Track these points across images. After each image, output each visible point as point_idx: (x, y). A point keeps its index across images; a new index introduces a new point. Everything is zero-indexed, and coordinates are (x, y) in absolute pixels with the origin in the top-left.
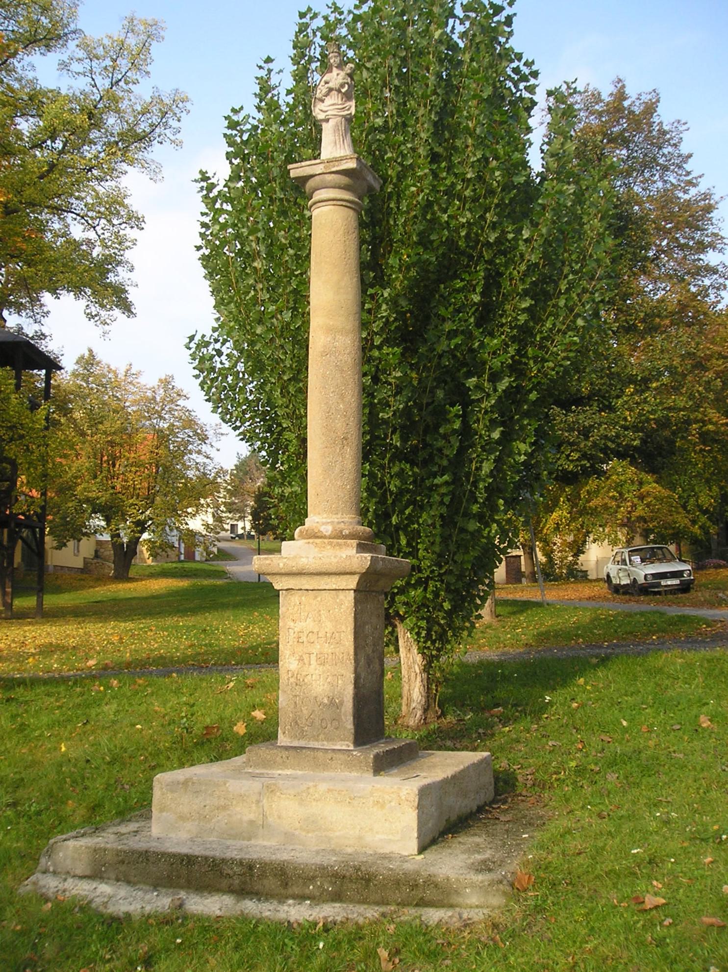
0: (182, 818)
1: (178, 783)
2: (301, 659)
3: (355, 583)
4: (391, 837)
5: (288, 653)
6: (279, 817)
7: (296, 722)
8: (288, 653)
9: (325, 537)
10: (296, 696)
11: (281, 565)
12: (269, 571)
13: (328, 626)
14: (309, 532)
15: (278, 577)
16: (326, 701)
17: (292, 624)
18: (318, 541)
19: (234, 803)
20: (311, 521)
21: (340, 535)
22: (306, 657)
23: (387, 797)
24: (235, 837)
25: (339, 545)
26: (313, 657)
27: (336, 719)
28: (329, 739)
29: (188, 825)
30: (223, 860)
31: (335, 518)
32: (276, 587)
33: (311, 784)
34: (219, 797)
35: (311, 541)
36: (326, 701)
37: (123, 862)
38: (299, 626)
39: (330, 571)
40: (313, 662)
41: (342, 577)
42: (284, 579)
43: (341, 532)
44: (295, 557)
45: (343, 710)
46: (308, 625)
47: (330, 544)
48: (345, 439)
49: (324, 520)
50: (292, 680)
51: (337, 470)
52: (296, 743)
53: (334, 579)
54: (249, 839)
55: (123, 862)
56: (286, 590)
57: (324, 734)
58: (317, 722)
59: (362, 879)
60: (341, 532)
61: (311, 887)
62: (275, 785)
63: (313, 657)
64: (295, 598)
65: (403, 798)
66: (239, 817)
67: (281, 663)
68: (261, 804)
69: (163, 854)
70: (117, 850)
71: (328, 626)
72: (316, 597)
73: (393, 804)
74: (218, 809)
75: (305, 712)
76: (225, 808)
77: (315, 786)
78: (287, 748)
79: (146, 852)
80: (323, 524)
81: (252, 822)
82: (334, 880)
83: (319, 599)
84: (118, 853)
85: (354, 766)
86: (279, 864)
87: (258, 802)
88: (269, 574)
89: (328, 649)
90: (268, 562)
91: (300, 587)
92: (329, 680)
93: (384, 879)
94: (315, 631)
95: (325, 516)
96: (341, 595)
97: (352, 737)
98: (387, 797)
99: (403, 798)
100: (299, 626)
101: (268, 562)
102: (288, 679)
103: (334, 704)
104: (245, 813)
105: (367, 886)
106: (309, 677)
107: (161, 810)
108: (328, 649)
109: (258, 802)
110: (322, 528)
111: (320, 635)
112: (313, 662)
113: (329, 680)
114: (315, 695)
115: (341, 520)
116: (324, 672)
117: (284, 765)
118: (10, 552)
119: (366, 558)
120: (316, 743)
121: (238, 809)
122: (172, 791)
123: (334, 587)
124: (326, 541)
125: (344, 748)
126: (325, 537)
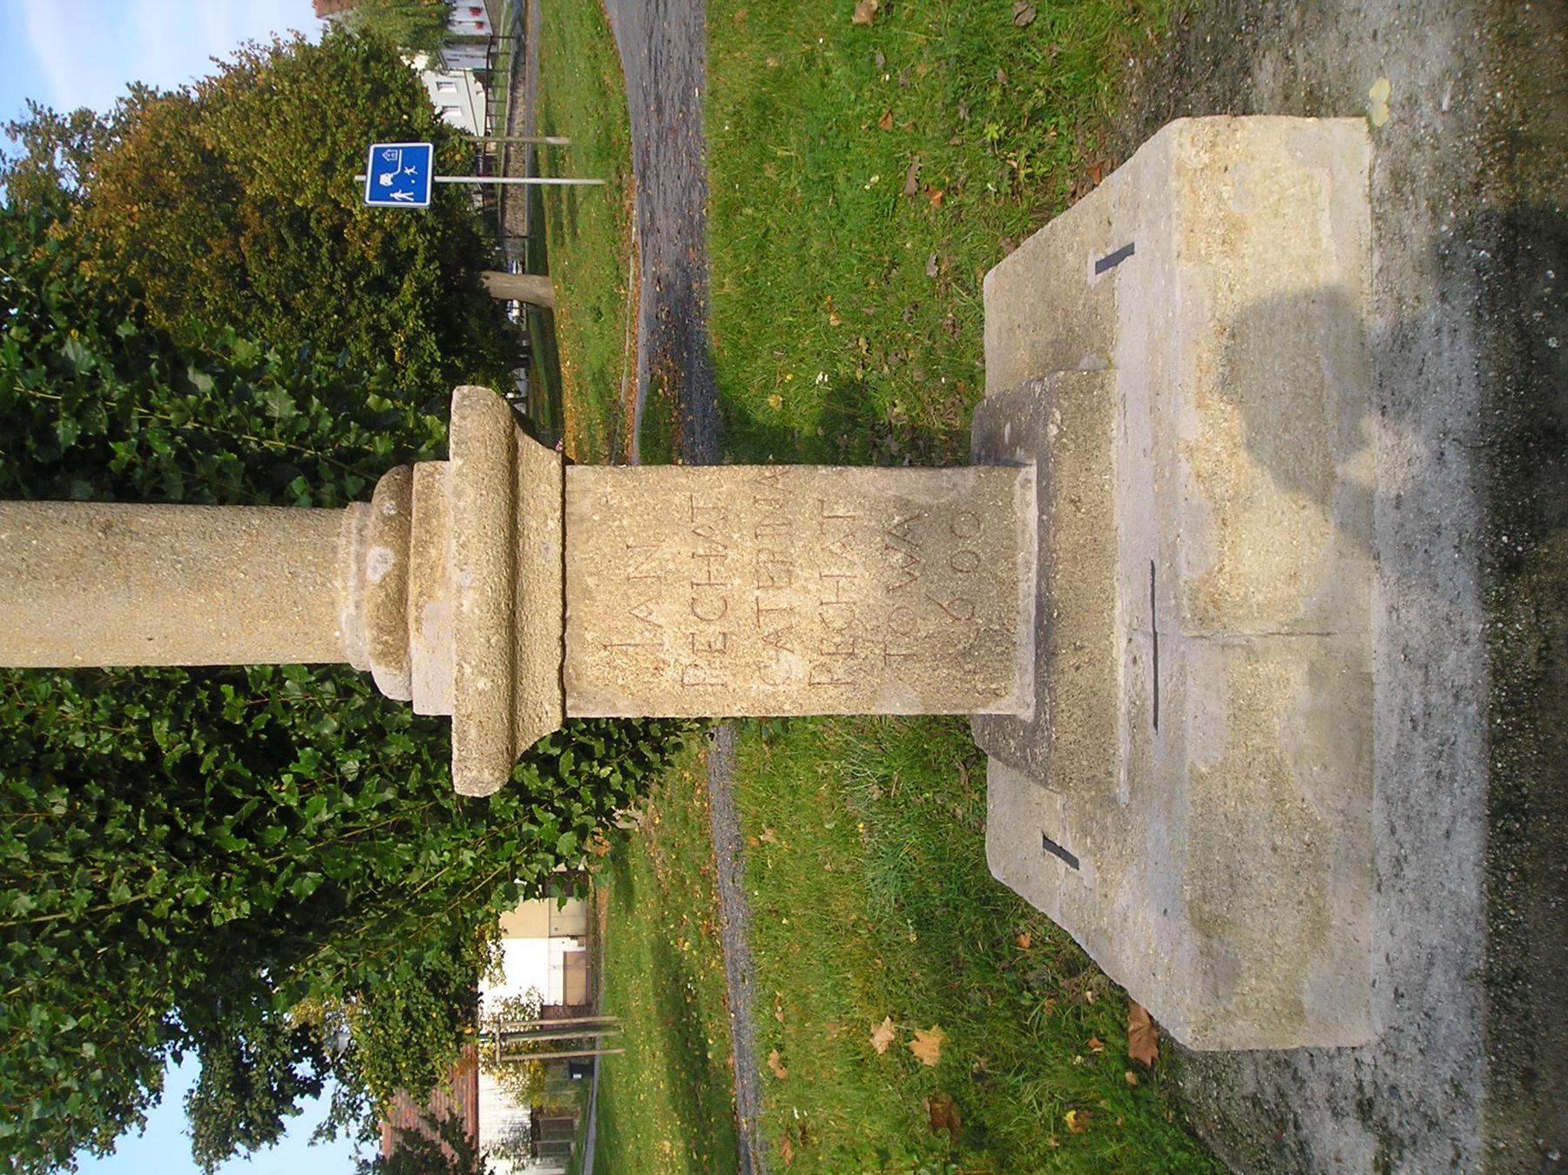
0: (1318, 929)
1: (1206, 952)
2: (775, 641)
3: (543, 452)
4: (1324, 200)
5: (756, 686)
6: (1294, 576)
7: (965, 654)
8: (756, 686)
9: (401, 575)
10: (886, 656)
11: (483, 684)
12: (500, 727)
13: (675, 549)
14: (385, 621)
15: (524, 712)
16: (898, 558)
17: (670, 673)
18: (413, 589)
19: (1258, 740)
20: (354, 644)
21: (400, 527)
22: (770, 625)
23: (1208, 211)
24: (1363, 734)
25: (426, 517)
26: (770, 599)
27: (951, 521)
28: (1007, 550)
29: (1338, 909)
30: (1497, 673)
31: (347, 547)
32: (553, 724)
33: (1185, 468)
34: (1245, 798)
35: (412, 612)
36: (898, 558)
37: (1529, 1076)
38: (676, 651)
39: (503, 519)
40: (783, 599)
41: (524, 492)
42: (528, 692)
43: (387, 519)
44: (459, 636)
45: (923, 499)
46: (668, 612)
47: (424, 544)
48: (107, 528)
49: (352, 583)
50: (839, 673)
51: (202, 548)
52: (1026, 655)
53: (528, 506)
54: (1366, 681)
55: (1529, 1076)
56: (562, 639)
57: (994, 561)
58: (960, 584)
59: (1510, 161)
60: (387, 519)
61: (1553, 343)
62: (1193, 598)
63: (770, 599)
64: (590, 663)
65: (1206, 158)
66: (1300, 721)
67: (790, 710)
68: (1258, 644)
69: (1495, 914)
70: (1491, 1102)
71: (675, 549)
72: (587, 593)
73: (1227, 191)
74: (1281, 801)
75: (931, 627)
76: (1277, 775)
77: (1190, 450)
78: (1043, 685)
79: (1489, 982)
80: (361, 572)
81: (1315, 675)
82: (1522, 261)
83: (591, 582)
84: (1500, 1099)
85: (1091, 429)
86: (1492, 462)
87: (1251, 653)
88: (513, 739)
89: (743, 552)
90: (473, 733)
91: (556, 643)
92: (836, 548)
93: (1502, 85)
94: (689, 593)
95: (338, 583)
96: (580, 505)
97: (1000, 473)
98: (1208, 211)
99: (1206, 158)
100: (676, 651)
101: (473, 733)
102: (835, 683)
103: (908, 533)
104: (1287, 688)
105: (1530, 143)
106: (830, 613)
107: (1296, 1012)
108: (743, 552)
109: (1251, 653)
110: (374, 577)
111: (702, 577)
112: (783, 599)
113: (836, 548)
114: (879, 593)
115: (354, 536)
116: (813, 564)
117: (1100, 661)
118: (146, 491)
119: (464, 397)
120: (1022, 586)
121: (1277, 725)
122: (1234, 976)
123: (554, 525)
124: (413, 562)
125: (1032, 495)
126: (401, 575)
